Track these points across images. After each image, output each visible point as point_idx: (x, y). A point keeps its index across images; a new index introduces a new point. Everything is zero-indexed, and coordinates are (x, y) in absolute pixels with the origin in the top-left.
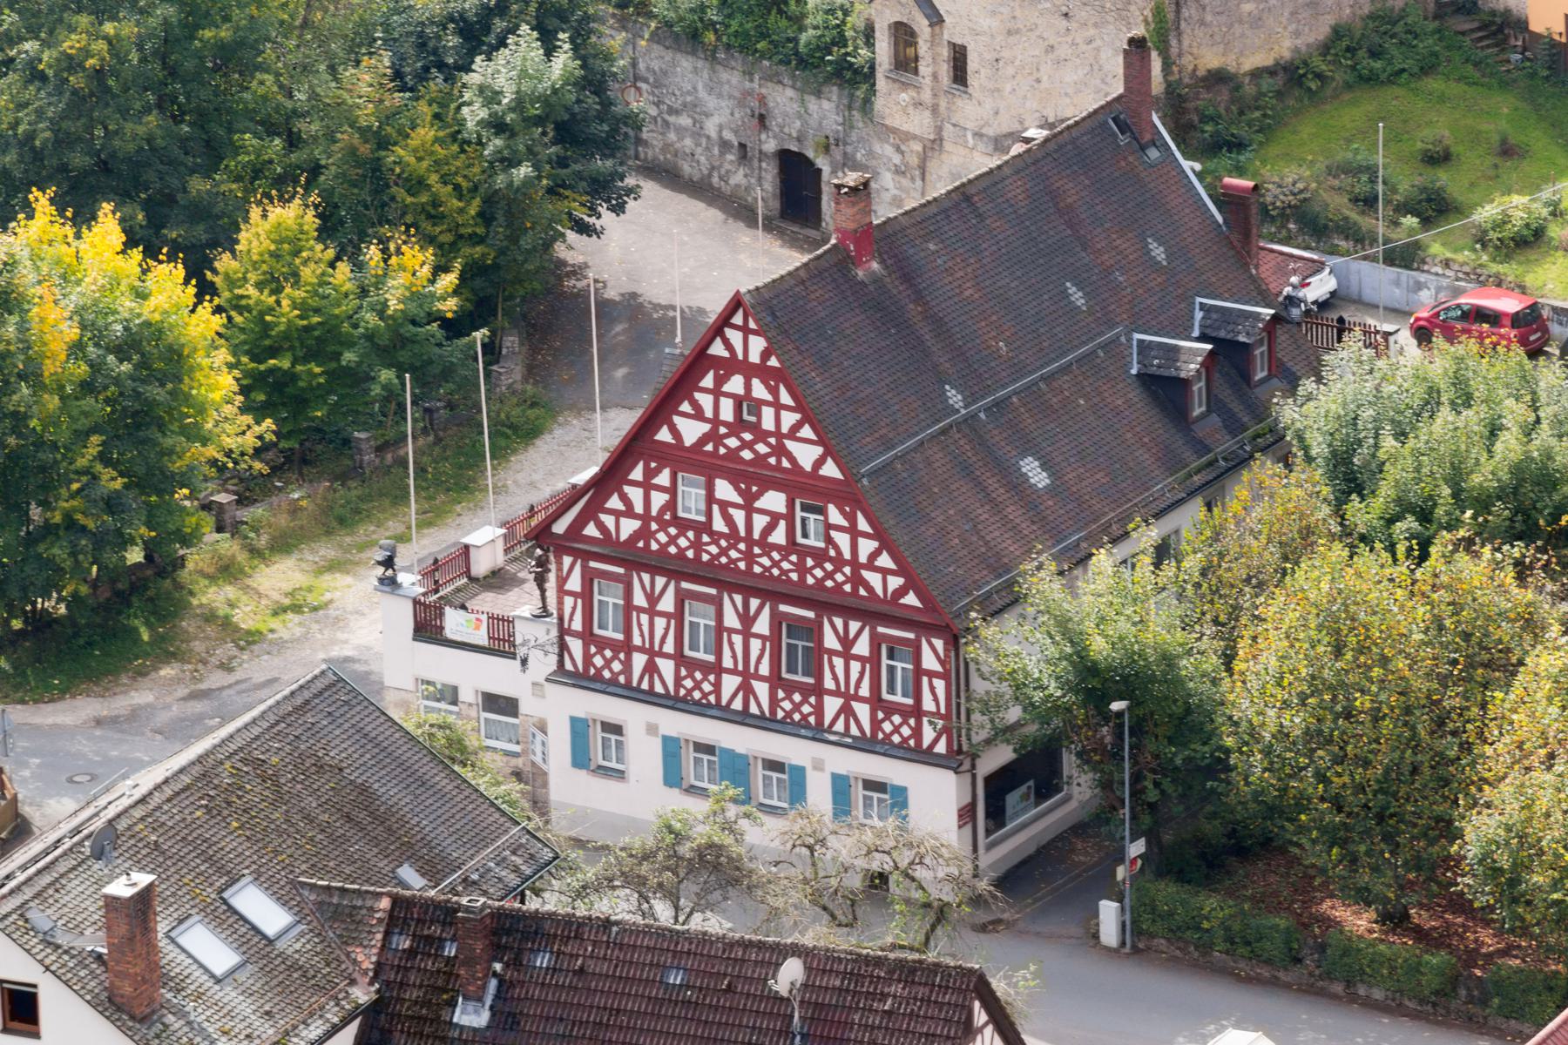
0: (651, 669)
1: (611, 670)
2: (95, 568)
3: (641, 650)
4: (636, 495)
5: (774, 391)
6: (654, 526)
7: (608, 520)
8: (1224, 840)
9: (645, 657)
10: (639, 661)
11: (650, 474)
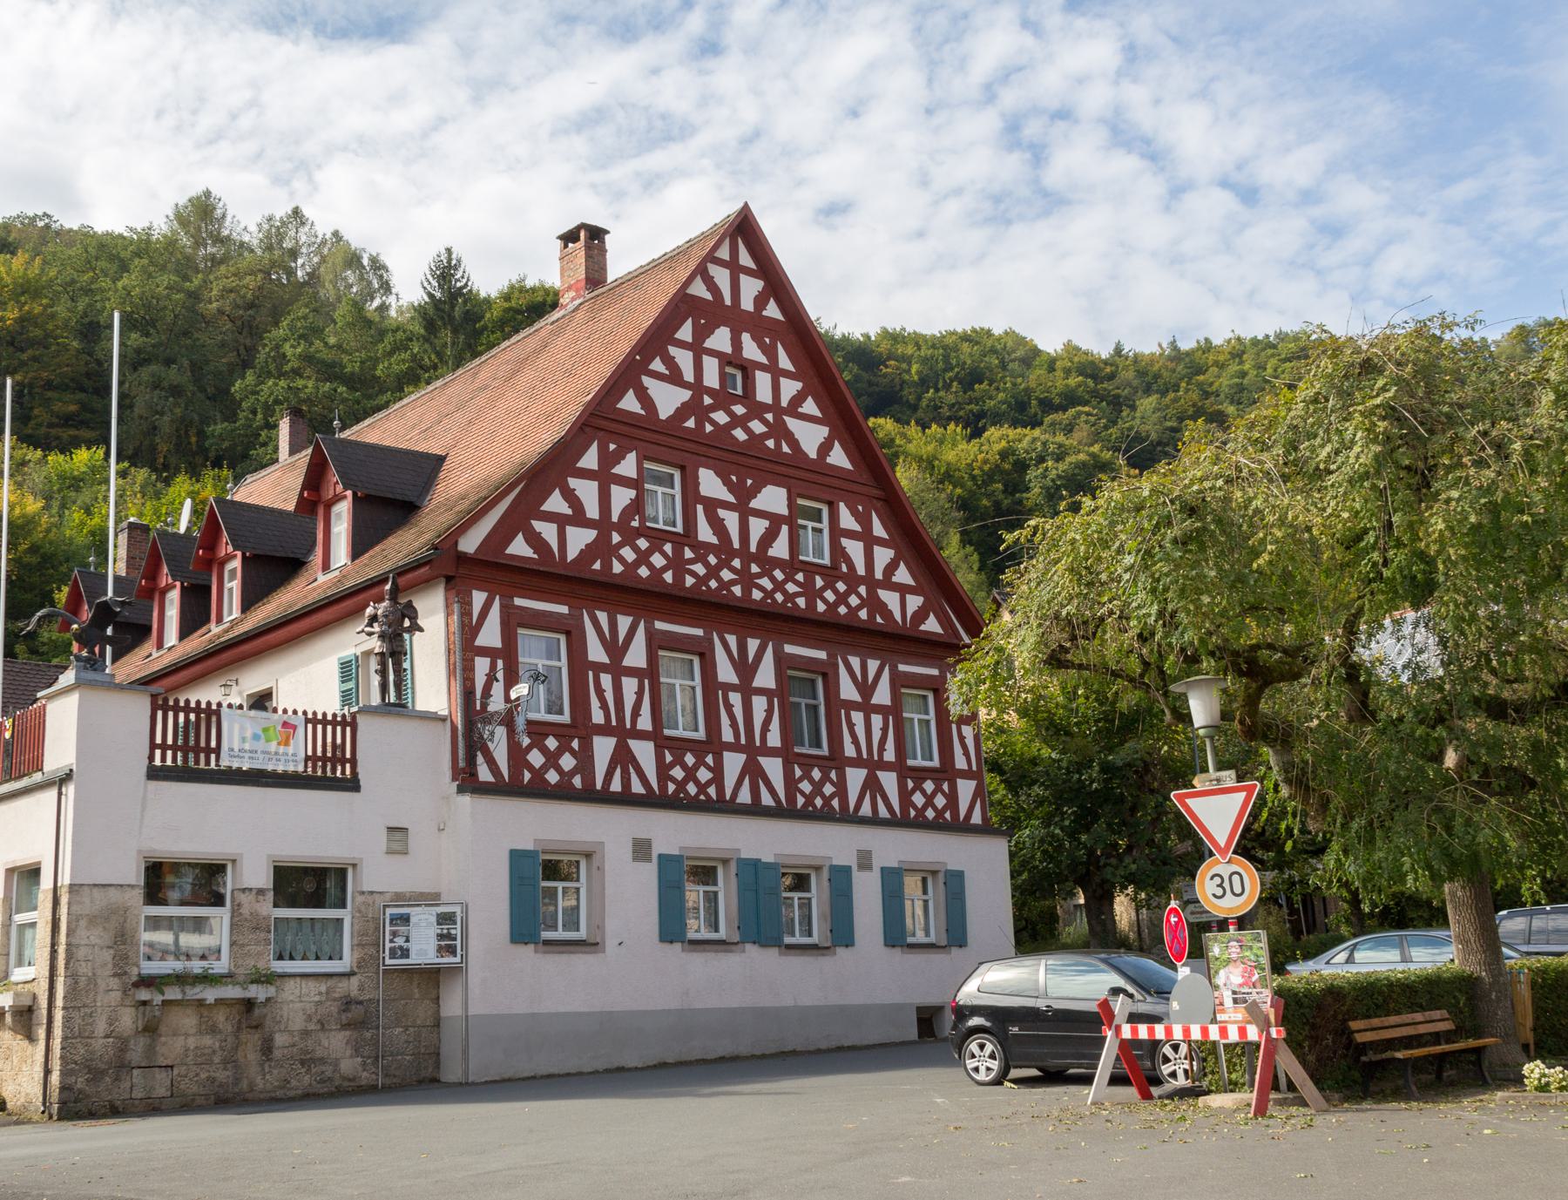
4: (587, 491)
5: (770, 353)
10: (603, 748)
11: (608, 460)
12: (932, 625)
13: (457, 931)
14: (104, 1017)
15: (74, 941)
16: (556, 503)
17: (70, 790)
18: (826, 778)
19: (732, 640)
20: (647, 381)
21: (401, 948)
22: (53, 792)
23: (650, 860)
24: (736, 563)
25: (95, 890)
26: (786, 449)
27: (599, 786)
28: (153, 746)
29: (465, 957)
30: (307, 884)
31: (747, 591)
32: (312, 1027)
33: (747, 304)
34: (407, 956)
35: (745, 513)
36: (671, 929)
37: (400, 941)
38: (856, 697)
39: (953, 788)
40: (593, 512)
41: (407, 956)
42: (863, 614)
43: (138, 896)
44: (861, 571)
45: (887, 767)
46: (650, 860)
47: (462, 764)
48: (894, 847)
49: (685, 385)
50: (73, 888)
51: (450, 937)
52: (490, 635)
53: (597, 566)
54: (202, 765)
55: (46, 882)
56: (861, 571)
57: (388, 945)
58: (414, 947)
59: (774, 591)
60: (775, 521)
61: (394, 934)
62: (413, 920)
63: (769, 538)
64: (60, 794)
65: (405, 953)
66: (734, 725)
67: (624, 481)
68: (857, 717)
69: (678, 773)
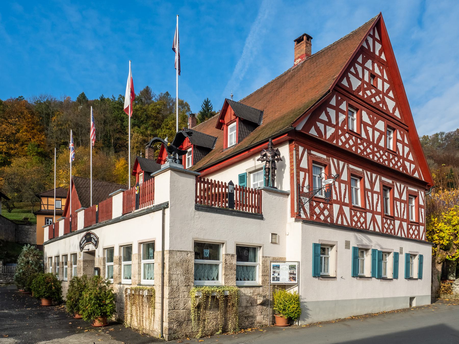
0: (341, 212)
1: (324, 215)
2: (70, 219)
3: (336, 202)
4: (333, 113)
5: (382, 72)
6: (340, 132)
7: (321, 126)
8: (34, 104)
9: (338, 206)
10: (336, 208)
11: (339, 103)
12: (416, 175)
13: (296, 272)
14: (182, 302)
15: (171, 273)
16: (323, 117)
17: (167, 211)
18: (325, 208)
19: (398, 184)
20: (350, 75)
21: (277, 277)
22: (161, 212)
23: (349, 249)
24: (371, 146)
25: (178, 253)
26: (385, 108)
27: (335, 222)
28: (197, 197)
29: (298, 281)
30: (245, 253)
31: (389, 164)
32: (249, 305)
33: (377, 53)
34: (279, 280)
35: (374, 129)
36: (356, 273)
37: (276, 275)
38: (398, 197)
39: (331, 208)
40: (334, 122)
41: (279, 280)
42: (401, 169)
43: (191, 256)
44: (401, 154)
45: (346, 205)
46: (349, 249)
47: (296, 211)
48: (409, 247)
49: (360, 79)
50: (170, 252)
51: (293, 274)
52: (304, 164)
53: (335, 142)
54: (250, 212)
55: (158, 247)
56: (401, 154)
57: (272, 276)
58: (281, 277)
59: (380, 158)
60: (381, 133)
61: (274, 272)
62: (280, 267)
63: (379, 139)
64: (164, 214)
65: (278, 279)
66: (336, 194)
67: (343, 112)
68: (370, 194)
69: (355, 219)
